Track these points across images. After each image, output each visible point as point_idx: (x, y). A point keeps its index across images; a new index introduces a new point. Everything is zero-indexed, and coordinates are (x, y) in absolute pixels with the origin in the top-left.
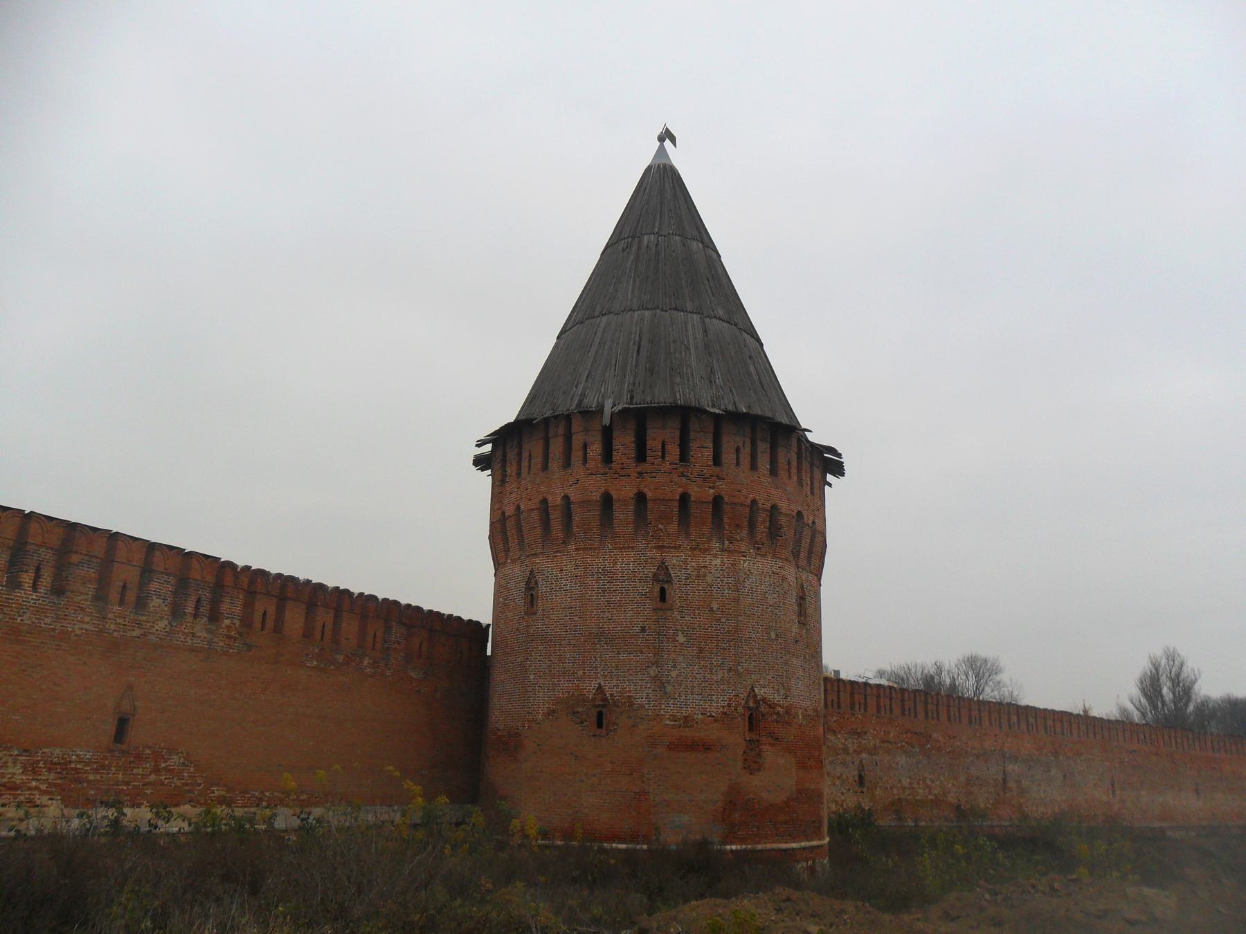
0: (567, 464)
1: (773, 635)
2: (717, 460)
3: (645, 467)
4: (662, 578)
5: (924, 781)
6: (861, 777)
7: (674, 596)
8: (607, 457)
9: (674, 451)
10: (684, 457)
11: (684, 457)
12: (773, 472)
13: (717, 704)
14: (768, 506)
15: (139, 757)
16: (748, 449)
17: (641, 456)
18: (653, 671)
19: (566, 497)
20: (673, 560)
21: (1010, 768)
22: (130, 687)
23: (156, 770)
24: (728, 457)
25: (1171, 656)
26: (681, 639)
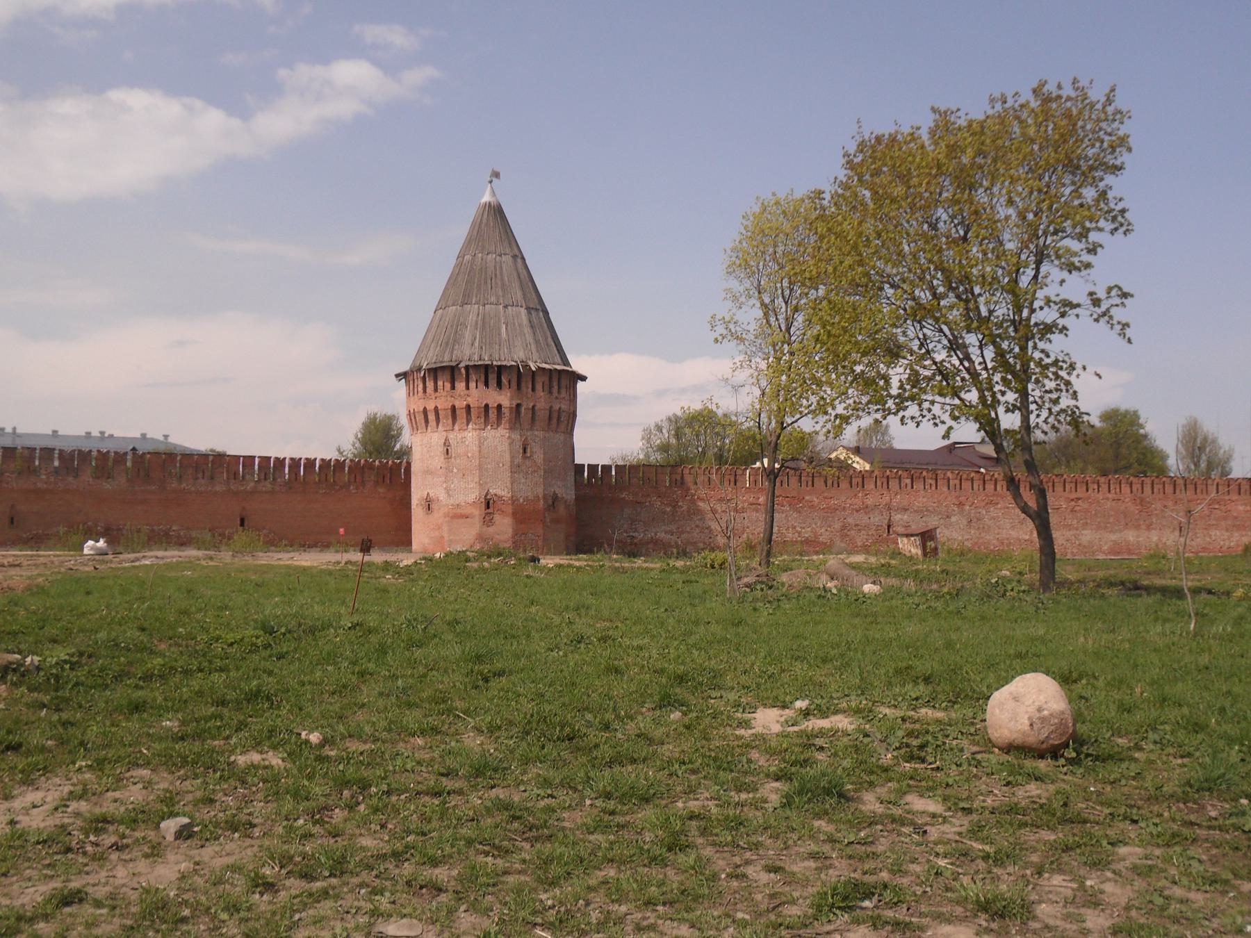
2: (468, 388)
4: (447, 444)
7: (452, 452)
9: (448, 385)
10: (453, 387)
17: (436, 390)
21: (897, 517)
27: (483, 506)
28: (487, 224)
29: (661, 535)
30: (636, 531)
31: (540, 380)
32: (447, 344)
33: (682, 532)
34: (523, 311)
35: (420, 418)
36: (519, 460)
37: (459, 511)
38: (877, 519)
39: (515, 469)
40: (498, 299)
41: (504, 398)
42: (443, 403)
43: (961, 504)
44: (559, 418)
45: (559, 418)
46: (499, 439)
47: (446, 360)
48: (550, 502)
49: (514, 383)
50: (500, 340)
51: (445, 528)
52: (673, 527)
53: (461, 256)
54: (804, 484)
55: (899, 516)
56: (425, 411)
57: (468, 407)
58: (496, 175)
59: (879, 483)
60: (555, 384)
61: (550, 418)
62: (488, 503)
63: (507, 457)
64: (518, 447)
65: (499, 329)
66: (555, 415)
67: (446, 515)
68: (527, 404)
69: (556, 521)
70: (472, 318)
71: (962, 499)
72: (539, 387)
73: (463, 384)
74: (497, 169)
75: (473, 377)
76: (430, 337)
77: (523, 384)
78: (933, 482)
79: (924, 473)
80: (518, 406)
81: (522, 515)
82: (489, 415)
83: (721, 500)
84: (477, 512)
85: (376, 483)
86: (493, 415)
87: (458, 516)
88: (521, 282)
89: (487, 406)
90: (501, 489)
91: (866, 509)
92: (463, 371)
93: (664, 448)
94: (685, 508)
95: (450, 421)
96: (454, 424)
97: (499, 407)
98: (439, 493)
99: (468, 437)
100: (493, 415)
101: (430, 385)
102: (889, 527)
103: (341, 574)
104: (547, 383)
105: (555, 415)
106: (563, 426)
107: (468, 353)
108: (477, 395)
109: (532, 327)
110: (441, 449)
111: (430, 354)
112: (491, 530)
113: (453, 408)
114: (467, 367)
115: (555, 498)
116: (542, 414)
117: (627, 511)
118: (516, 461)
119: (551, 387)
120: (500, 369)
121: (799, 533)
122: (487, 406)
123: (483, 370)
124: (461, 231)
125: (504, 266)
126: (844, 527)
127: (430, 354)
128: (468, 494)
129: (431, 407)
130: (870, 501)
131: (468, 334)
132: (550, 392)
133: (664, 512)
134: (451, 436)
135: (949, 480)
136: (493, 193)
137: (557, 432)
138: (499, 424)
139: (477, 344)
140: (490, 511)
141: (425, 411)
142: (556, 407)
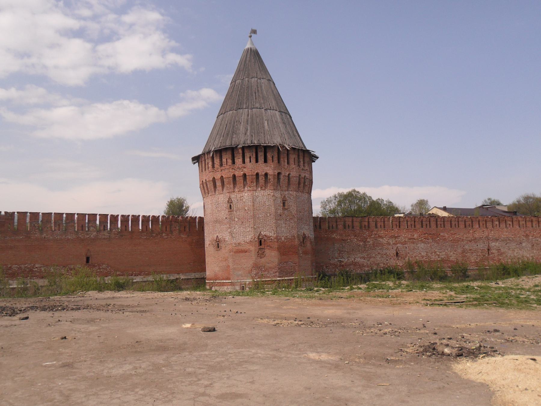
0: (205, 170)
1: (269, 215)
2: (244, 162)
3: (223, 168)
4: (230, 201)
5: (435, 252)
6: (397, 253)
7: (234, 207)
8: (213, 166)
9: (230, 161)
10: (234, 162)
11: (234, 162)
12: (265, 161)
13: (249, 238)
14: (264, 174)
15: (94, 266)
16: (254, 156)
17: (221, 165)
18: (229, 230)
19: (214, 178)
20: (233, 196)
21: (493, 244)
22: (89, 250)
23: (100, 269)
24: (247, 160)
25: (427, 201)
26: (236, 220)
27: (257, 244)
28: (250, 61)
29: (358, 260)
30: (343, 257)
31: (293, 157)
32: (228, 134)
33: (370, 258)
34: (277, 113)
35: (210, 185)
36: (280, 211)
37: (240, 248)
38: (481, 246)
39: (278, 217)
40: (261, 105)
41: (270, 169)
42: (227, 173)
43: (527, 236)
44: (304, 183)
45: (304, 183)
46: (266, 197)
47: (228, 144)
48: (302, 240)
49: (276, 159)
50: (264, 131)
51: (230, 260)
52: (365, 255)
53: (234, 81)
54: (439, 226)
55: (494, 244)
56: (214, 180)
57: (245, 175)
58: (254, 32)
59: (481, 224)
60: (301, 160)
61: (299, 184)
62: (261, 242)
63: (273, 209)
64: (279, 201)
65: (263, 124)
66: (302, 180)
67: (231, 251)
68: (285, 173)
69: (305, 253)
70: (244, 117)
71: (527, 232)
72: (292, 161)
73: (241, 160)
74: (254, 28)
75: (247, 155)
76: (216, 132)
77: (282, 159)
78: (511, 223)
79: (506, 218)
80: (279, 174)
81: (285, 249)
82: (259, 180)
83: (391, 237)
84: (253, 248)
85: (180, 232)
86: (262, 180)
87: (239, 251)
88: (274, 95)
89: (257, 174)
90: (269, 232)
91: (475, 240)
92: (240, 151)
93: (333, 211)
94: (371, 242)
95: (232, 186)
96: (234, 187)
97: (266, 175)
98: (225, 236)
99: (245, 196)
100: (262, 180)
101: (217, 161)
102: (488, 250)
103: (74, 220)
104: (297, 159)
105: (302, 180)
106: (307, 188)
107: (243, 138)
108: (251, 167)
109: (284, 123)
110: (226, 205)
111: (216, 142)
112: (263, 260)
113: (234, 176)
114: (243, 148)
115: (305, 237)
116: (294, 180)
117: (337, 245)
118: (279, 212)
119: (299, 162)
120: (266, 148)
121: (439, 255)
122: (257, 174)
123: (254, 150)
124: (235, 63)
125: (263, 85)
126: (463, 252)
127: (216, 142)
128: (245, 235)
129: (218, 176)
130: (477, 235)
131: (242, 128)
132: (299, 166)
133: (359, 245)
134: (233, 196)
135: (519, 221)
136: (252, 43)
137: (303, 192)
138: (266, 187)
139: (248, 133)
140: (262, 247)
141: (214, 180)
142: (303, 175)
